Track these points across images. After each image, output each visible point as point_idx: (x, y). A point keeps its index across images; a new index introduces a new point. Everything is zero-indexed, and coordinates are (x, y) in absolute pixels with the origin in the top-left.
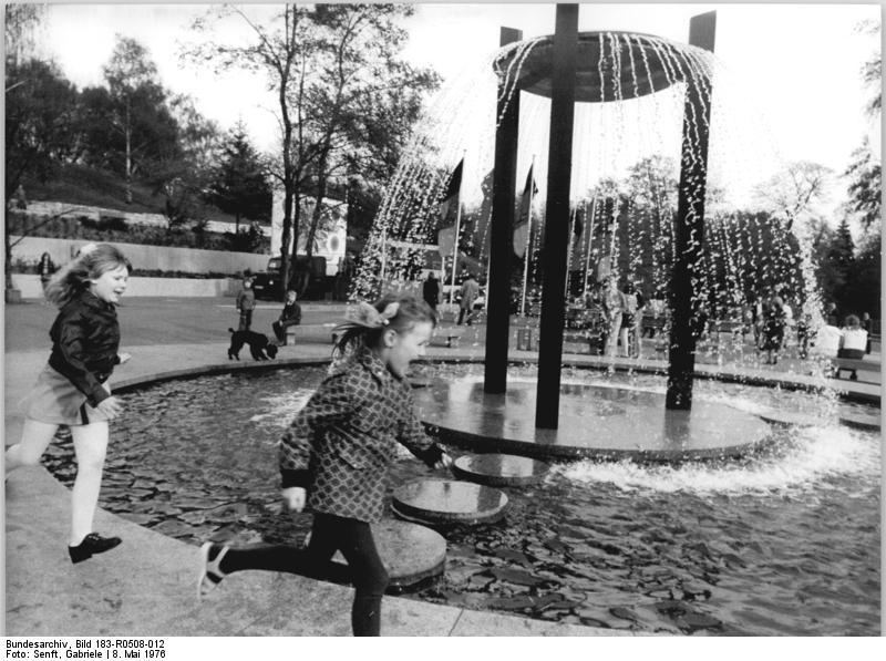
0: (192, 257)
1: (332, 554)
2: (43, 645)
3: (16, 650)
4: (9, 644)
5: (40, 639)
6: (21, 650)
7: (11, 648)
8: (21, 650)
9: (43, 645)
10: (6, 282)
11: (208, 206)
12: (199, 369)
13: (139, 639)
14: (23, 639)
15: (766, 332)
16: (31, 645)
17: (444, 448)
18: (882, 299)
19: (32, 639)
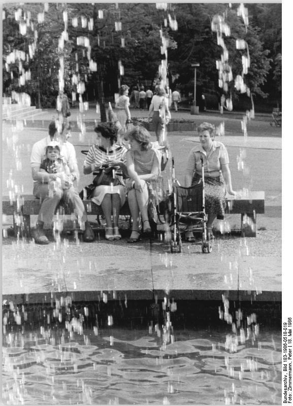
0: (32, 223)
1: (188, 94)
2: (286, 386)
3: (288, 399)
4: (285, 402)
5: (283, 388)
6: (288, 396)
7: (287, 401)
8: (288, 396)
9: (286, 386)
10: (3, 341)
11: (131, 137)
12: (206, 115)
13: (283, 346)
14: (283, 396)
15: (101, 335)
16: (285, 392)
17: (255, 295)
18: (208, 3)
19: (283, 391)
